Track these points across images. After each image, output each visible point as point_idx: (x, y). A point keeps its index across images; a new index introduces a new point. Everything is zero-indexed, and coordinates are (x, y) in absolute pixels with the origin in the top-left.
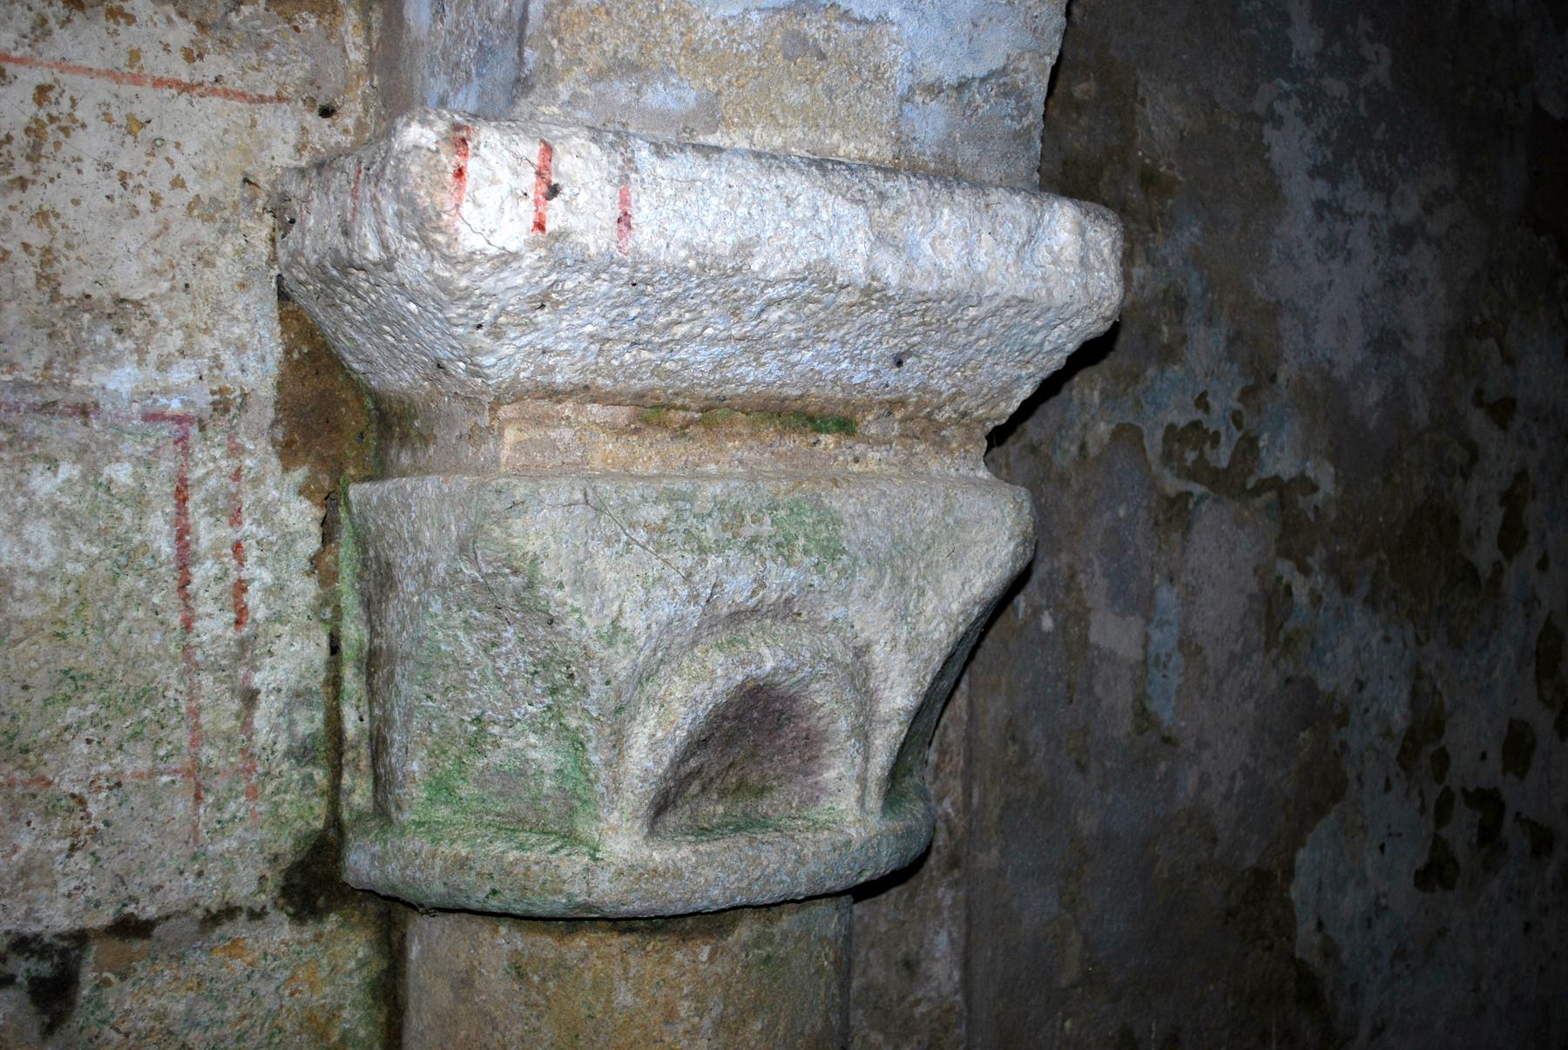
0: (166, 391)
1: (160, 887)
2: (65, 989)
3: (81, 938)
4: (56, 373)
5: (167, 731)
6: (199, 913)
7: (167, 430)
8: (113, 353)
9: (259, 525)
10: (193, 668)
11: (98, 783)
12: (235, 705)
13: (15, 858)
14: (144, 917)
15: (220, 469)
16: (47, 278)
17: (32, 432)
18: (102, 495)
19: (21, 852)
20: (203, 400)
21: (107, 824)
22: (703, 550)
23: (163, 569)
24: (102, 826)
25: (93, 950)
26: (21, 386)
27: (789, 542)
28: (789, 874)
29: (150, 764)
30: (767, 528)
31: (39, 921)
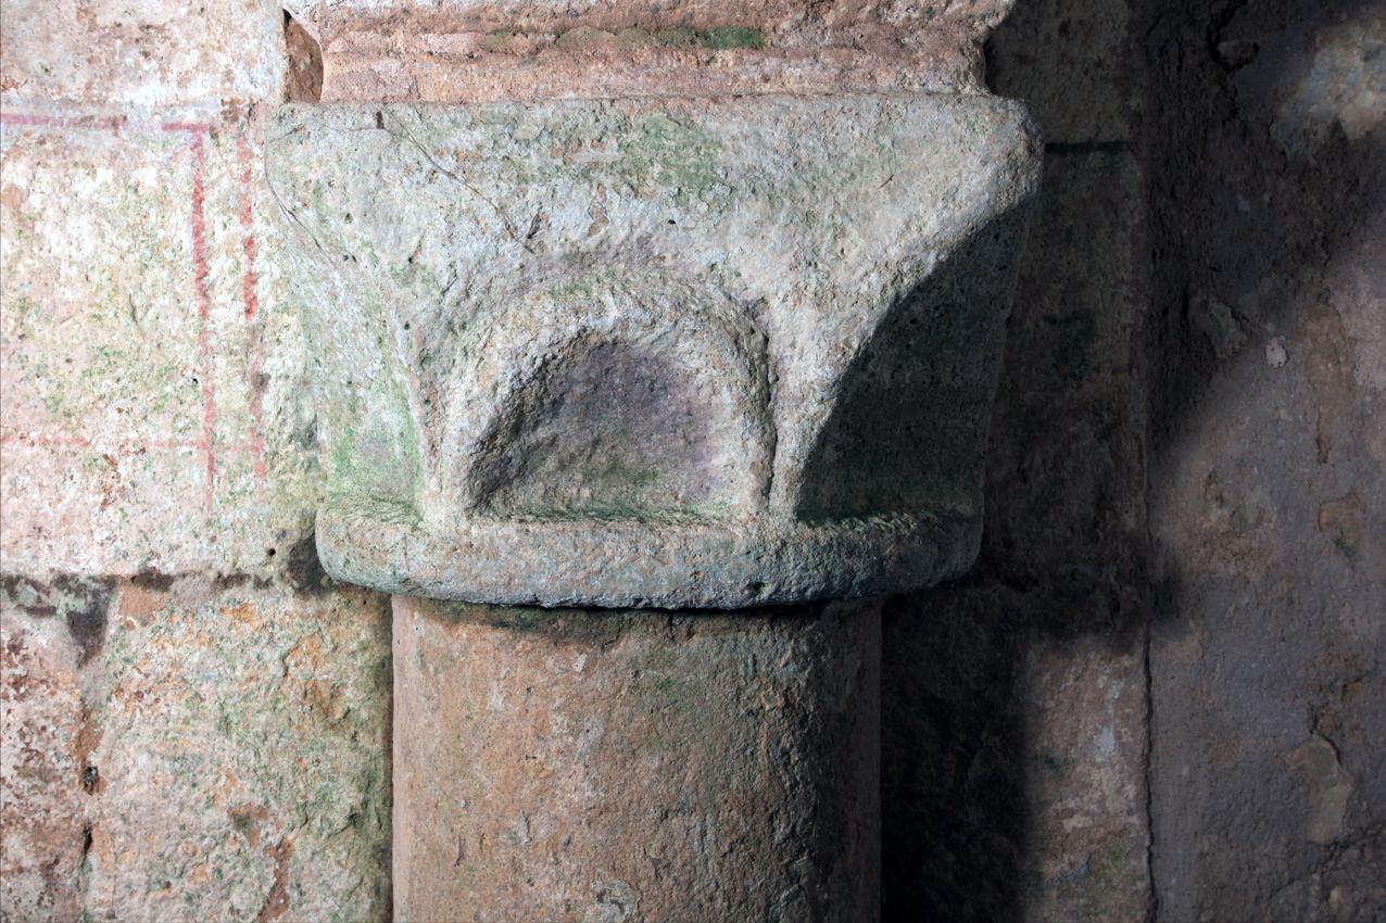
0: (185, 104)
1: (178, 547)
2: (99, 625)
3: (111, 582)
4: (95, 92)
5: (185, 406)
6: (212, 575)
7: (184, 137)
8: (140, 73)
9: (269, 224)
10: (208, 351)
11: (126, 448)
12: (246, 388)
13: (59, 506)
14: (164, 572)
15: (231, 172)
16: (86, 11)
17: (72, 142)
18: (132, 197)
19: (65, 501)
20: (214, 112)
21: (134, 485)
22: (522, 179)
23: (183, 262)
24: (130, 486)
25: (121, 592)
26: (68, 103)
27: (639, 170)
28: (642, 571)
29: (170, 435)
30: (611, 152)
31: (78, 563)
